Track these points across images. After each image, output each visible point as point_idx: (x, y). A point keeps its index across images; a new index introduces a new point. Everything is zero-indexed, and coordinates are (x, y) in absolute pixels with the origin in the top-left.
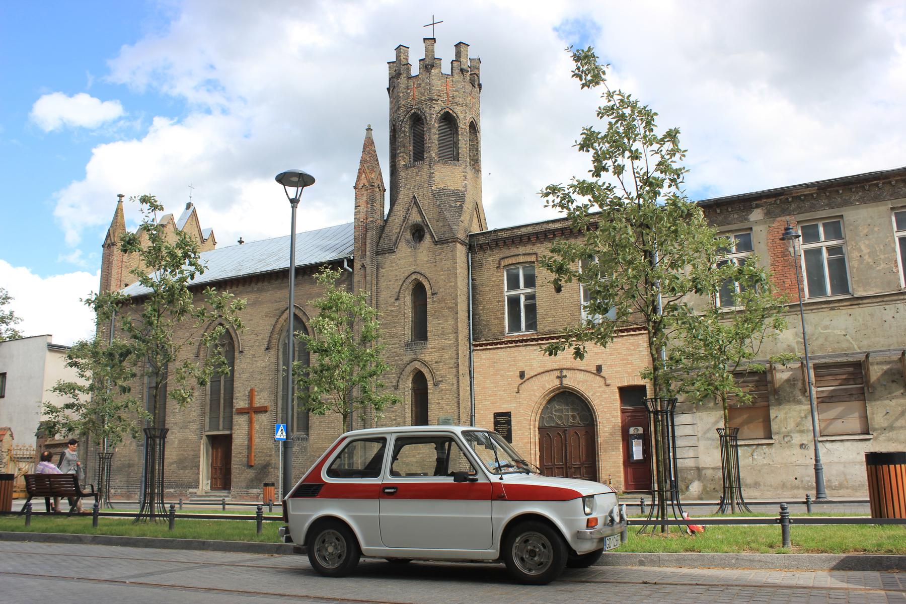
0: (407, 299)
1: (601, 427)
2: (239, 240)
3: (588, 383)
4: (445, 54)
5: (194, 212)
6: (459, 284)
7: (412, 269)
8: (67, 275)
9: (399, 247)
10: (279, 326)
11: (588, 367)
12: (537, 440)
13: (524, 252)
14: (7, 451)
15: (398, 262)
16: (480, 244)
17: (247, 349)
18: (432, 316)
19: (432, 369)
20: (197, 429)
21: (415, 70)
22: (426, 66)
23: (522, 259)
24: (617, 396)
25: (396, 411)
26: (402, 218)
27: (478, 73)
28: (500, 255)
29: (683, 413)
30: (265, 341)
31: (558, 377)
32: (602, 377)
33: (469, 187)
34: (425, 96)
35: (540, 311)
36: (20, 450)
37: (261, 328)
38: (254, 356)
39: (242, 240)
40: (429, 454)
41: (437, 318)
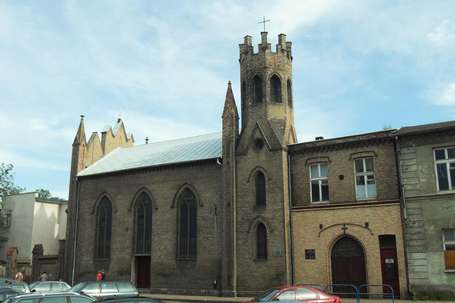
0: (253, 182)
1: (369, 259)
2: (146, 139)
3: (361, 233)
4: (273, 40)
5: (122, 124)
6: (284, 174)
7: (257, 164)
9: (249, 152)
10: (179, 195)
11: (361, 224)
12: (330, 265)
13: (321, 156)
14: (14, 260)
15: (248, 160)
16: (295, 151)
17: (160, 207)
18: (268, 192)
19: (269, 223)
20: (130, 252)
21: (256, 50)
22: (262, 48)
23: (320, 160)
24: (378, 241)
25: (248, 246)
26: (250, 135)
27: (290, 50)
28: (306, 158)
29: (418, 252)
30: (171, 203)
31: (342, 229)
32: (369, 229)
33: (288, 118)
34: (262, 65)
35: (331, 191)
36: (22, 260)
37: (168, 195)
38: (164, 212)
39: (148, 138)
40: (268, 271)
41: (272, 193)
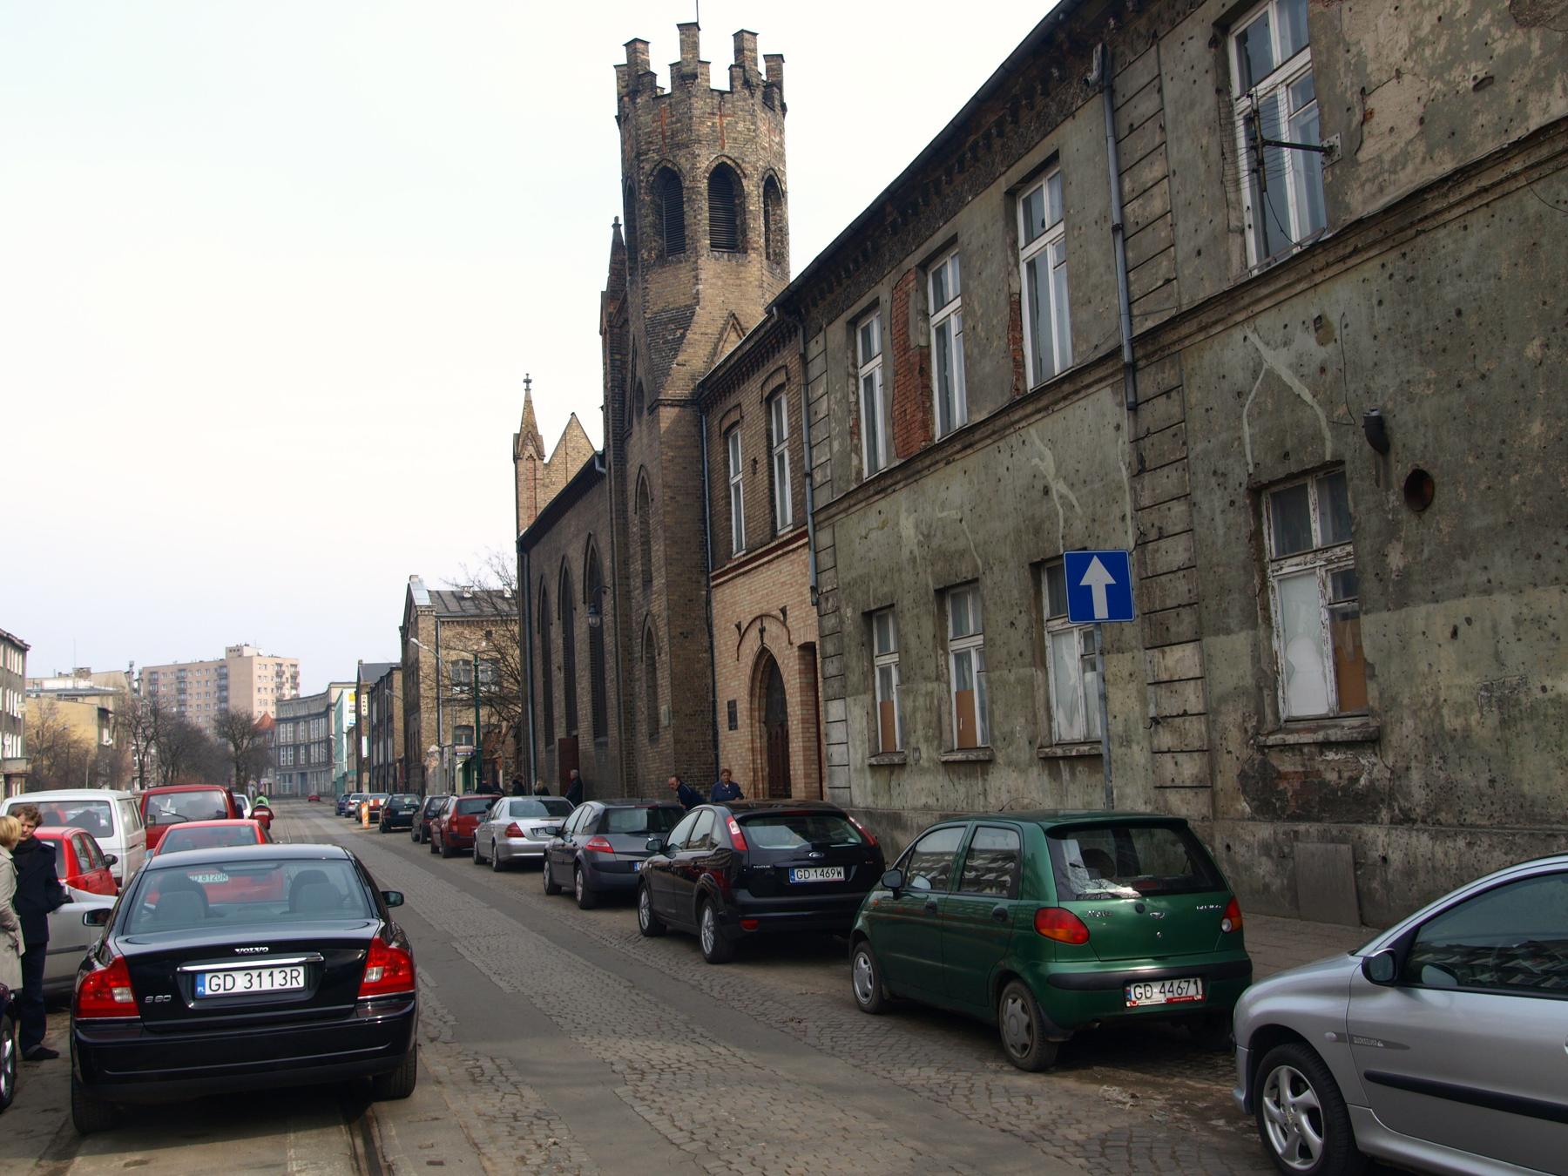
8: (598, 340)
21: (664, 82)
